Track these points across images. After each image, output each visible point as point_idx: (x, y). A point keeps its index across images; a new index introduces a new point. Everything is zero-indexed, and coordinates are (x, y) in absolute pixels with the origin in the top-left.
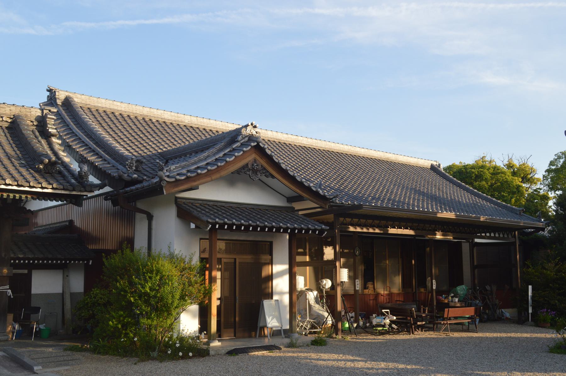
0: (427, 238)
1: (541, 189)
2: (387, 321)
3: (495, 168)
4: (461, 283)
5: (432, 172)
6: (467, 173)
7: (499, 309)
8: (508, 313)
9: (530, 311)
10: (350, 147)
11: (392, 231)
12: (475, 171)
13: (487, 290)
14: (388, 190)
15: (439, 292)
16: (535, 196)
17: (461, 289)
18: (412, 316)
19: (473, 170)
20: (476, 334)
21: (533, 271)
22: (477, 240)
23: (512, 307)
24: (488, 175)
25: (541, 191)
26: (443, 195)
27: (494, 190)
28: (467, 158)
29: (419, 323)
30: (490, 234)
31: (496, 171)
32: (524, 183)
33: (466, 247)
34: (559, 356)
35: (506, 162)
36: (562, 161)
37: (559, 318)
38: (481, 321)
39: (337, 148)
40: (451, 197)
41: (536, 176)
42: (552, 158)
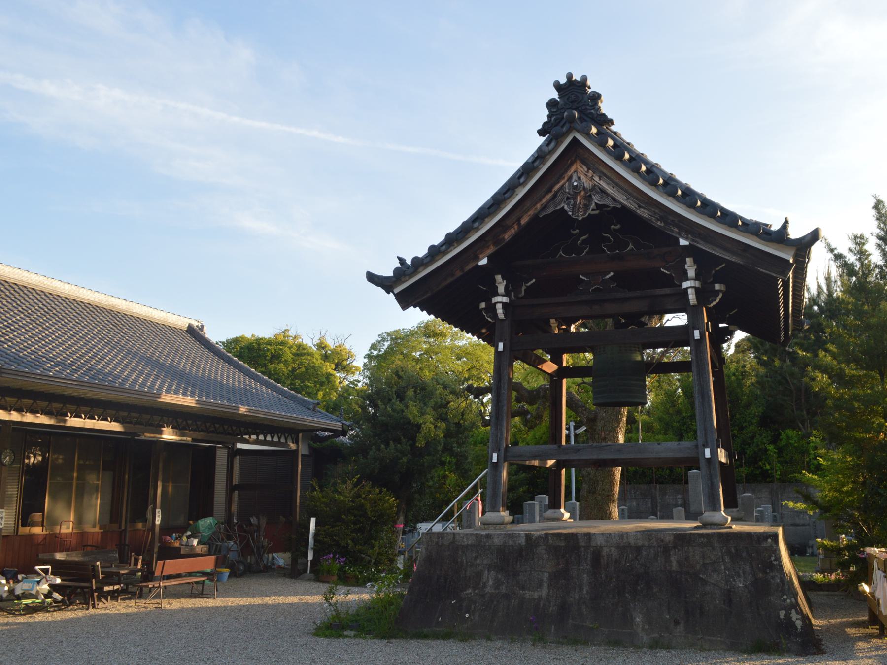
0: (143, 438)
1: (359, 382)
2: (45, 587)
3: (300, 346)
4: (209, 513)
5: (188, 336)
6: (259, 349)
7: (268, 553)
8: (282, 559)
9: (310, 557)
10: (42, 278)
11: (73, 422)
12: (272, 349)
13: (251, 524)
14: (95, 355)
15: (167, 529)
16: (351, 390)
17: (205, 523)
18: (96, 576)
19: (269, 347)
20: (211, 600)
21: (320, 495)
22: (240, 446)
23: (285, 551)
24: (289, 356)
25: (360, 384)
26: (197, 371)
27: (296, 378)
28: (260, 328)
29: (106, 588)
30: (265, 437)
31: (301, 351)
32: (338, 371)
33: (222, 456)
34: (327, 641)
35: (316, 341)
36: (387, 344)
37: (350, 568)
38: (233, 575)
39: (16, 277)
40: (210, 374)
41: (355, 364)
42: (374, 339)
